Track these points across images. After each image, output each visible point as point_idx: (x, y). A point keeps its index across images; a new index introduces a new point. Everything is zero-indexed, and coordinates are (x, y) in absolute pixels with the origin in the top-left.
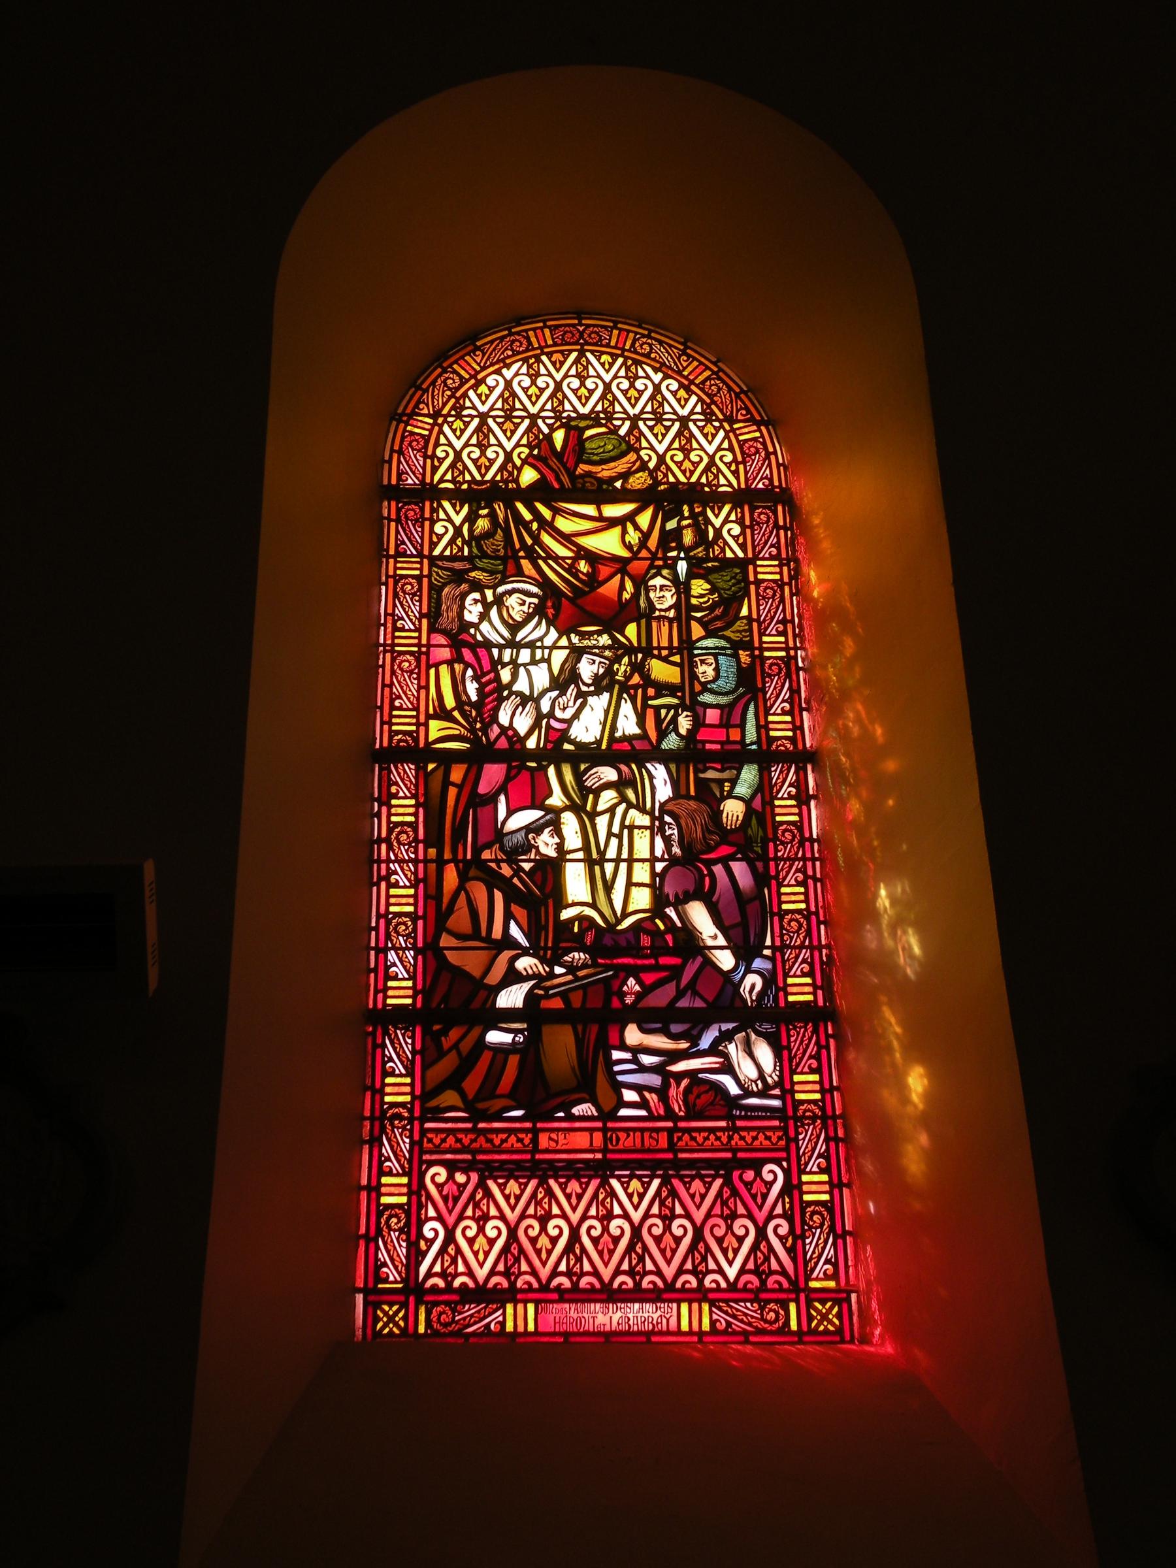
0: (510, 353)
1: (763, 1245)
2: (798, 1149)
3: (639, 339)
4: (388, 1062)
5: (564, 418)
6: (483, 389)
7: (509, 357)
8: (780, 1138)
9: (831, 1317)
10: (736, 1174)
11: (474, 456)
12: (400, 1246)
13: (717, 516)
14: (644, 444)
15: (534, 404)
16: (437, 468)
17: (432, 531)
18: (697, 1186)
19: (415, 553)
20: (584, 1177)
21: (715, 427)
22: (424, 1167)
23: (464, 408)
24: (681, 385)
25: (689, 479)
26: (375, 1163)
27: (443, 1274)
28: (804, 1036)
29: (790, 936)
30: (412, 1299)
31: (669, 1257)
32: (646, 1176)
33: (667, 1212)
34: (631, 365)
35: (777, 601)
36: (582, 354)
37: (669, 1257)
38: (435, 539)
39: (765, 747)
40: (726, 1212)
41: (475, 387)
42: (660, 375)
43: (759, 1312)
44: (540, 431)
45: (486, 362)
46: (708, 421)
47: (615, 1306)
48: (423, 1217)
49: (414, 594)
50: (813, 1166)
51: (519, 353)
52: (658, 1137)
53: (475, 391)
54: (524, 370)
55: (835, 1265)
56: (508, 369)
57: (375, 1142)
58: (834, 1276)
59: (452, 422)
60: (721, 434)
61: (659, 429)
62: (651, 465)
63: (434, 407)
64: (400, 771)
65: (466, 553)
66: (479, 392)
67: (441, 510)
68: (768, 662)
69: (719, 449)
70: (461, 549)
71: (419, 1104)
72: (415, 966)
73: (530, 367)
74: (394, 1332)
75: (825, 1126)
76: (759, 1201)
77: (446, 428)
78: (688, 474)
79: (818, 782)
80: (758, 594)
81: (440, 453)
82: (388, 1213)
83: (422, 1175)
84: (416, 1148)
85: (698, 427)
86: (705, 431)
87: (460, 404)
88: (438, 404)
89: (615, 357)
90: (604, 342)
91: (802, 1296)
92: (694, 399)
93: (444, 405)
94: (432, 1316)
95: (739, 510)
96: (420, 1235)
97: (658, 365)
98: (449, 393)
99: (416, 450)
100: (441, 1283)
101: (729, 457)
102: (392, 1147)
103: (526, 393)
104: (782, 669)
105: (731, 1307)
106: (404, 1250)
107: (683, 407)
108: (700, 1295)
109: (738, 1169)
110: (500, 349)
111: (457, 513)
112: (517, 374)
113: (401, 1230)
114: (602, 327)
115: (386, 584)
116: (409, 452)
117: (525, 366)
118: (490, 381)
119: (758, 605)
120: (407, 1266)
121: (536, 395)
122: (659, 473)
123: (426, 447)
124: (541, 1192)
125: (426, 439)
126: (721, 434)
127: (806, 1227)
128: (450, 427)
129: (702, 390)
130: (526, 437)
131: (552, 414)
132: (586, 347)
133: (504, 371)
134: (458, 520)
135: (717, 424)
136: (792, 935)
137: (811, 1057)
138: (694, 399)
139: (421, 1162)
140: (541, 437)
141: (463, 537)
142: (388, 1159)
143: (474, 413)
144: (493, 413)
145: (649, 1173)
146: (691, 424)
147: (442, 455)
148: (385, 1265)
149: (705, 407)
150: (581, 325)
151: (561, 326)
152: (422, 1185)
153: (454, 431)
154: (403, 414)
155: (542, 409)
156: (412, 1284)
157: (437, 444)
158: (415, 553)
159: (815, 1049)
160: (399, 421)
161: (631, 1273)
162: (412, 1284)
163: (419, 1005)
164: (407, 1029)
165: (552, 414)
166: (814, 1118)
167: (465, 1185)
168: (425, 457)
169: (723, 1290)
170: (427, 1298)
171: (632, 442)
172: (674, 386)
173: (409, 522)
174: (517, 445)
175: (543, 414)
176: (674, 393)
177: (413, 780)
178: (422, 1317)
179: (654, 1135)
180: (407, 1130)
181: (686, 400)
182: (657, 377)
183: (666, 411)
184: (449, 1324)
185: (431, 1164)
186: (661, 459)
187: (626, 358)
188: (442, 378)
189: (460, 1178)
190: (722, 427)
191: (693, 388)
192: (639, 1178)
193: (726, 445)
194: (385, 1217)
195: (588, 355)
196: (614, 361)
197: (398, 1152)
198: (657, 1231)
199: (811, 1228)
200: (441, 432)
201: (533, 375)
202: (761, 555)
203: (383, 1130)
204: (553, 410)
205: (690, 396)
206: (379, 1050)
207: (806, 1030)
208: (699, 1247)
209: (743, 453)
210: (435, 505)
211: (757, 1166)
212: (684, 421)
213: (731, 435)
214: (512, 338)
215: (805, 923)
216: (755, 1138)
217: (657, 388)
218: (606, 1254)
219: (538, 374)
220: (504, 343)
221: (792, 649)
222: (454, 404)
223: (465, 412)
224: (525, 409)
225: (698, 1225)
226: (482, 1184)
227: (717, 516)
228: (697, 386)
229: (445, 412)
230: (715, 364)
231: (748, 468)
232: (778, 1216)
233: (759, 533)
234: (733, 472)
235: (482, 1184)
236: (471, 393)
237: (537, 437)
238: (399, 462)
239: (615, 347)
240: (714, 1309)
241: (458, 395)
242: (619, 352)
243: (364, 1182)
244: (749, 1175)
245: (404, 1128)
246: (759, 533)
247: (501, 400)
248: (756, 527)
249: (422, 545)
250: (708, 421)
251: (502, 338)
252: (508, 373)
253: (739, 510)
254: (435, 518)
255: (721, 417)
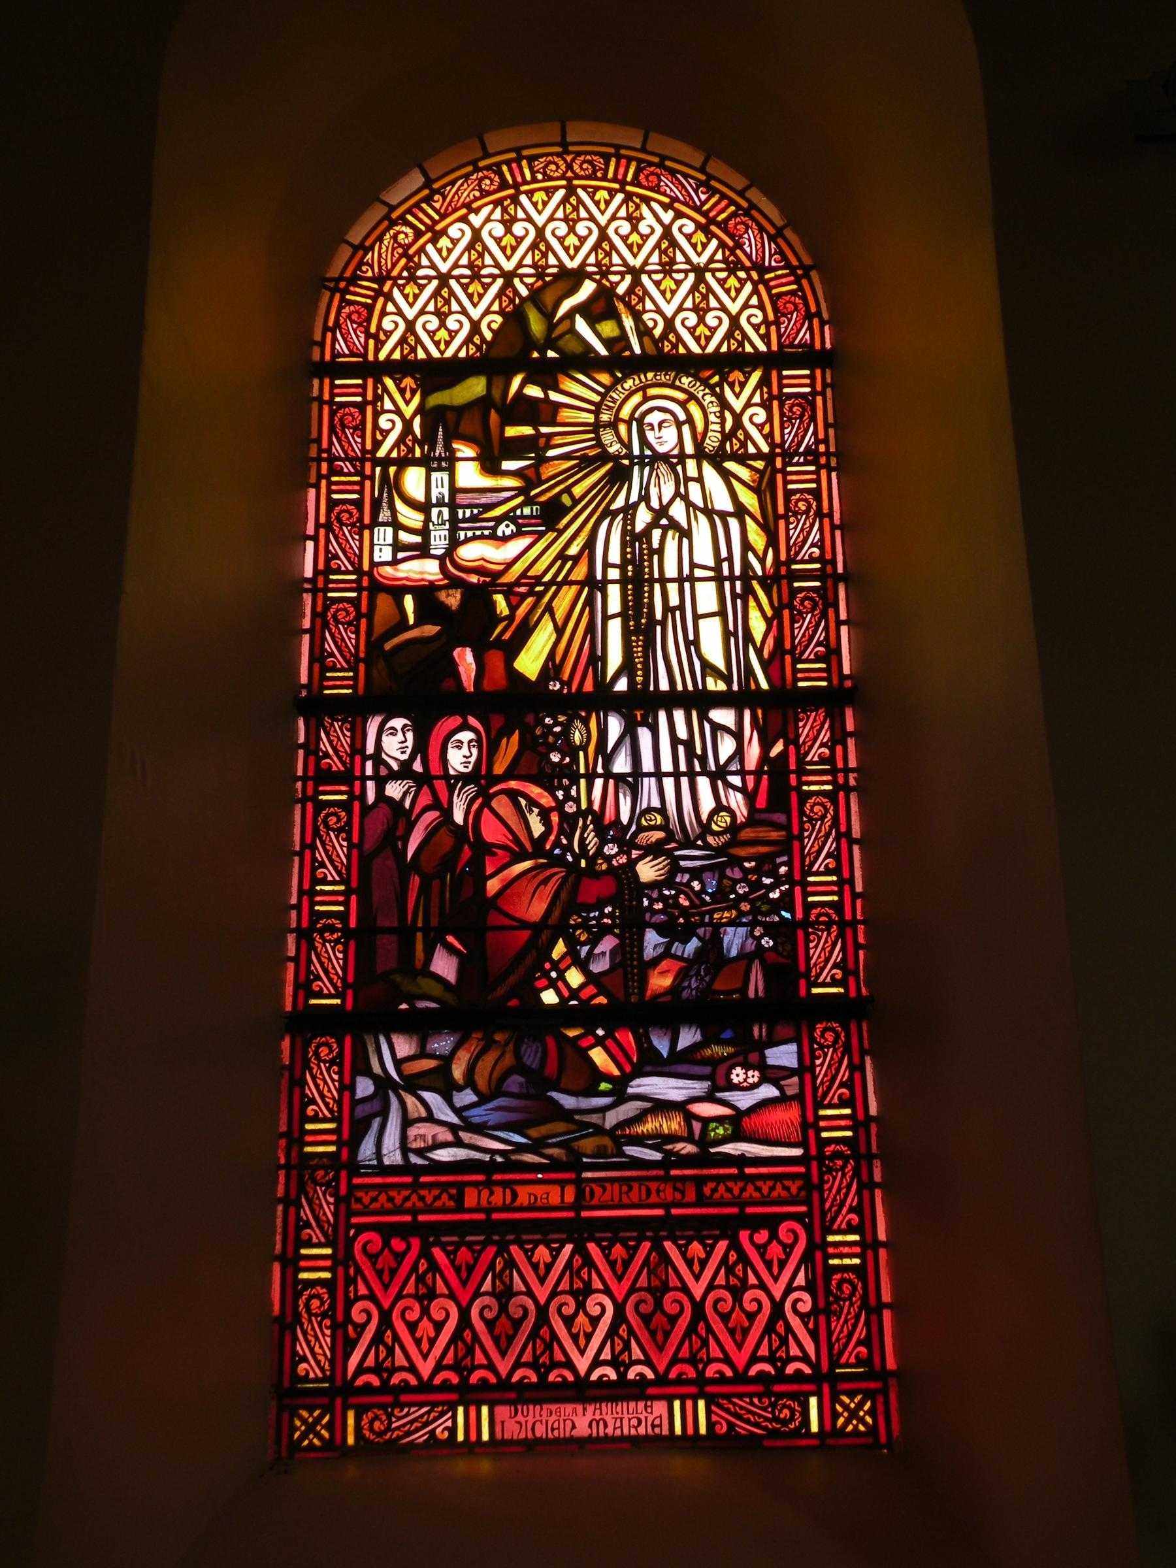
0: (477, 194)
1: (737, 333)
2: (815, 1078)
3: (644, 168)
4: (314, 980)
5: (549, 275)
6: (444, 242)
7: (476, 199)
8: (800, 1189)
9: (846, 1414)
10: (744, 1235)
11: (430, 327)
12: (324, 1334)
13: (737, 396)
14: (649, 305)
15: (508, 258)
16: (384, 343)
17: (376, 426)
18: (618, 1251)
19: (350, 568)
20: (529, 1242)
21: (739, 280)
22: (352, 1232)
23: (419, 266)
24: (699, 226)
25: (703, 349)
26: (296, 1109)
27: (377, 1369)
28: (820, 831)
29: (817, 935)
30: (339, 1402)
31: (660, 1343)
32: (632, 1239)
33: (657, 1283)
34: (509, 205)
35: (833, 935)
36: (571, 190)
37: (660, 1343)
38: (379, 437)
39: (774, 374)
40: (422, 1290)
41: (434, 241)
42: (671, 214)
43: (770, 1409)
44: (516, 293)
45: (447, 209)
46: (732, 270)
47: (525, 1407)
48: (352, 1295)
49: (350, 624)
50: (834, 1095)
51: (489, 193)
52: (684, 1187)
53: (435, 246)
54: (497, 214)
55: (822, 548)
56: (476, 214)
57: (291, 1203)
58: (836, 871)
59: (404, 286)
60: (749, 287)
61: (475, 288)
62: (657, 332)
63: (380, 267)
64: (310, 1338)
65: (418, 453)
66: (439, 246)
67: (386, 397)
68: (814, 911)
69: (746, 306)
70: (411, 450)
71: (350, 1040)
72: (348, 867)
73: (505, 210)
74: (314, 1444)
75: (841, 935)
76: (776, 1271)
77: (396, 293)
78: (703, 342)
79: (848, 560)
80: (782, 415)
81: (387, 324)
82: (342, 411)
83: (350, 1242)
84: (342, 1207)
85: (718, 280)
86: (470, 290)
87: (414, 262)
88: (386, 263)
89: (612, 193)
90: (599, 174)
91: (826, 1388)
92: (714, 243)
93: (394, 265)
94: (363, 1423)
95: (765, 390)
96: (348, 1319)
97: (667, 200)
98: (400, 250)
99: (355, 323)
100: (375, 1381)
101: (758, 318)
102: (312, 1211)
103: (562, 244)
104: (840, 1035)
105: (735, 1404)
106: (328, 1340)
107: (572, 258)
108: (700, 1387)
109: (745, 1228)
110: (465, 190)
111: (407, 403)
112: (488, 220)
113: (332, 1062)
114: (596, 154)
115: (315, 538)
116: (347, 325)
117: (499, 210)
118: (454, 231)
119: (782, 428)
120: (332, 1362)
121: (511, 246)
122: (666, 343)
123: (369, 320)
124: (423, 1265)
125: (370, 308)
126: (749, 287)
127: (805, 819)
128: (402, 292)
129: (725, 231)
130: (497, 302)
131: (659, 268)
132: (576, 182)
133: (472, 217)
134: (408, 411)
135: (742, 274)
136: (820, 933)
137: (842, 1085)
138: (714, 243)
139: (349, 1226)
140: (517, 301)
141: (414, 435)
142: (318, 978)
143: (432, 273)
144: (456, 272)
145: (609, 1235)
146: (516, 281)
147: (387, 426)
148: (307, 1225)
149: (727, 253)
150: (569, 153)
151: (541, 156)
152: (350, 1255)
153: (406, 297)
154: (341, 278)
155: (520, 265)
156: (339, 1383)
157: (384, 313)
158: (350, 568)
159: (841, 956)
160: (333, 292)
161: (614, 1363)
162: (339, 1383)
163: (349, 1006)
164: (344, 721)
165: (659, 268)
166: (828, 925)
167: (402, 1255)
168: (368, 336)
169: (651, 1383)
170: (353, 1400)
171: (633, 302)
172: (690, 227)
173: (341, 626)
174: (487, 312)
175: (521, 271)
176: (689, 237)
177: (345, 861)
178: (351, 1421)
179: (679, 1185)
180: (357, 527)
181: (704, 246)
182: (667, 217)
183: (712, 1355)
184: (384, 1432)
185: (361, 1228)
186: (669, 324)
187: (629, 197)
188: (392, 232)
189: (398, 1244)
190: (750, 278)
191: (713, 228)
192: (470, 1245)
193: (754, 301)
194: (304, 1297)
195: (580, 191)
196: (612, 197)
197: (347, 549)
198: (645, 1309)
199: (821, 1047)
200: (389, 297)
201: (507, 221)
202: (799, 558)
203: (302, 1190)
204: (534, 265)
205: (709, 241)
206: (297, 1090)
207: (829, 935)
208: (621, 1331)
209: (776, 310)
210: (380, 391)
211: (771, 1223)
212: (699, 272)
213: (761, 288)
214: (481, 174)
215: (815, 504)
216: (772, 1189)
217: (667, 230)
218: (581, 1340)
219: (514, 219)
220: (469, 182)
221: (840, 771)
222: (406, 264)
223: (420, 273)
224: (497, 265)
225: (698, 1300)
226: (426, 1253)
227: (737, 396)
228: (718, 225)
229: (395, 273)
230: (741, 193)
231: (783, 330)
232: (799, 1288)
233: (795, 528)
234: (762, 337)
235: (426, 1253)
236: (430, 248)
237: (512, 301)
238: (328, 541)
239: (614, 180)
240: (713, 1408)
241: (411, 252)
242: (616, 186)
243: (300, 773)
244: (762, 1236)
245: (337, 941)
246: (795, 528)
247: (657, 251)
248: (792, 519)
249: (360, 557)
250: (732, 270)
251: (467, 177)
252: (476, 220)
253: (765, 390)
254: (379, 408)
255: (748, 264)
